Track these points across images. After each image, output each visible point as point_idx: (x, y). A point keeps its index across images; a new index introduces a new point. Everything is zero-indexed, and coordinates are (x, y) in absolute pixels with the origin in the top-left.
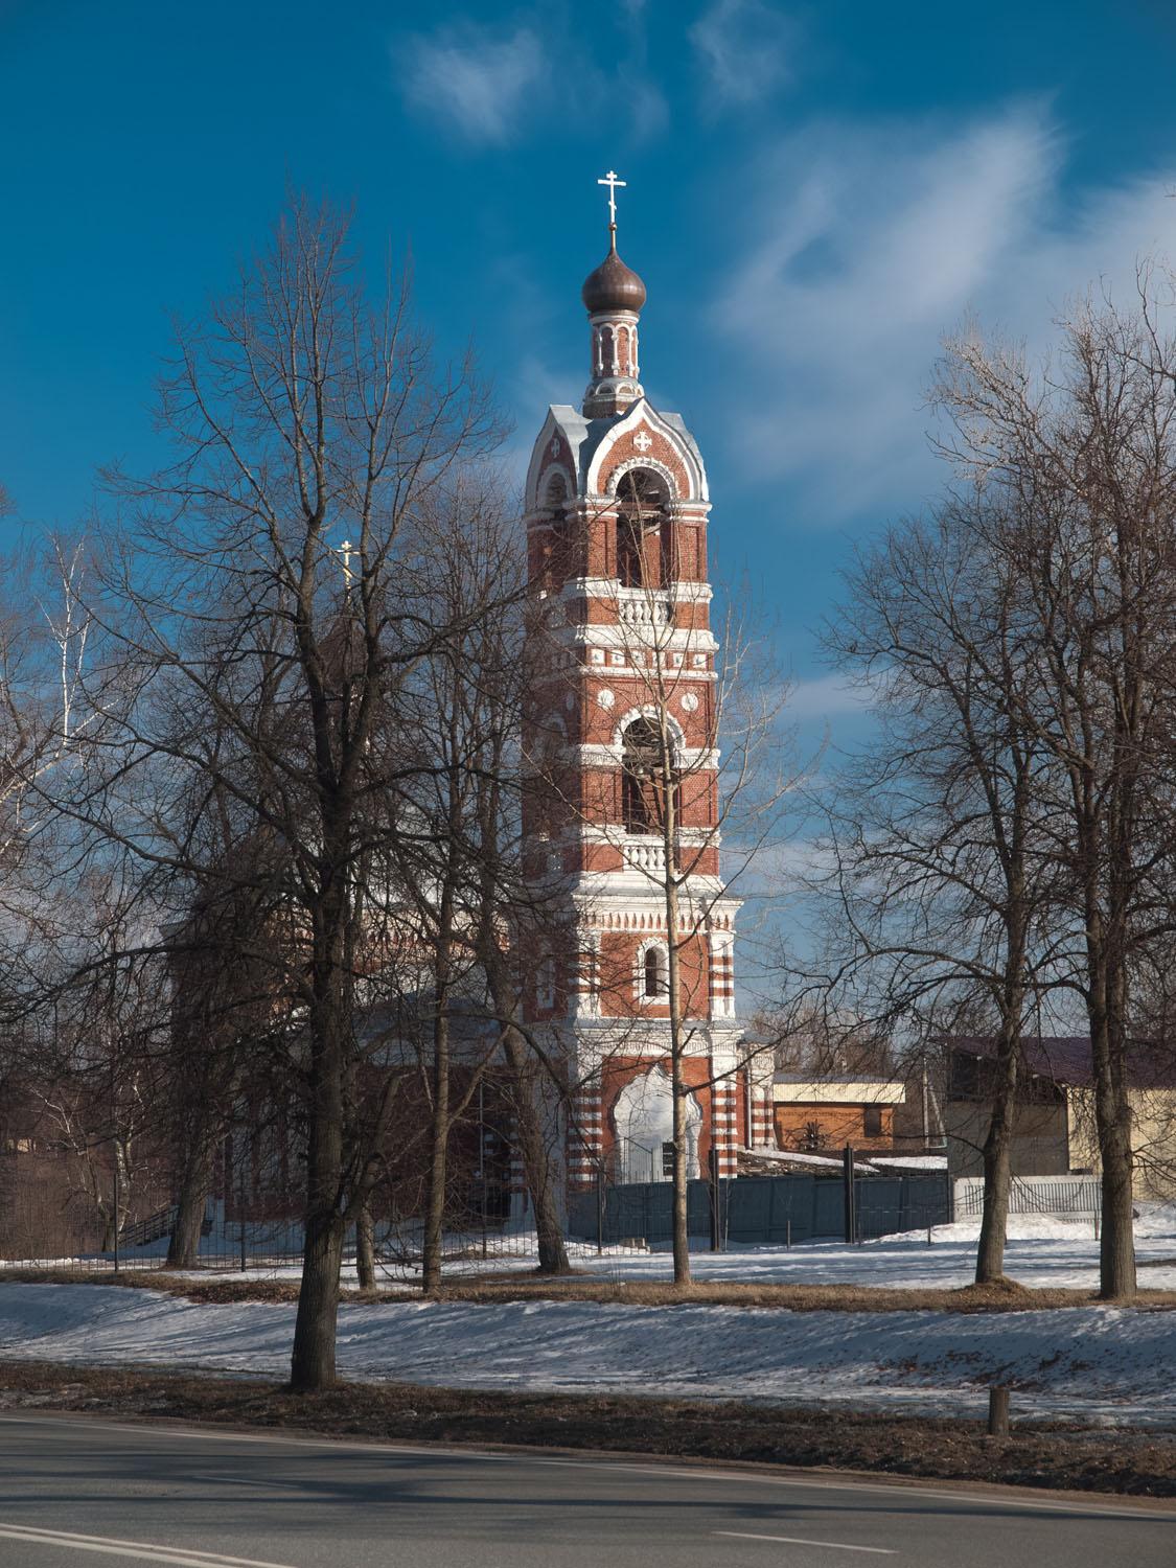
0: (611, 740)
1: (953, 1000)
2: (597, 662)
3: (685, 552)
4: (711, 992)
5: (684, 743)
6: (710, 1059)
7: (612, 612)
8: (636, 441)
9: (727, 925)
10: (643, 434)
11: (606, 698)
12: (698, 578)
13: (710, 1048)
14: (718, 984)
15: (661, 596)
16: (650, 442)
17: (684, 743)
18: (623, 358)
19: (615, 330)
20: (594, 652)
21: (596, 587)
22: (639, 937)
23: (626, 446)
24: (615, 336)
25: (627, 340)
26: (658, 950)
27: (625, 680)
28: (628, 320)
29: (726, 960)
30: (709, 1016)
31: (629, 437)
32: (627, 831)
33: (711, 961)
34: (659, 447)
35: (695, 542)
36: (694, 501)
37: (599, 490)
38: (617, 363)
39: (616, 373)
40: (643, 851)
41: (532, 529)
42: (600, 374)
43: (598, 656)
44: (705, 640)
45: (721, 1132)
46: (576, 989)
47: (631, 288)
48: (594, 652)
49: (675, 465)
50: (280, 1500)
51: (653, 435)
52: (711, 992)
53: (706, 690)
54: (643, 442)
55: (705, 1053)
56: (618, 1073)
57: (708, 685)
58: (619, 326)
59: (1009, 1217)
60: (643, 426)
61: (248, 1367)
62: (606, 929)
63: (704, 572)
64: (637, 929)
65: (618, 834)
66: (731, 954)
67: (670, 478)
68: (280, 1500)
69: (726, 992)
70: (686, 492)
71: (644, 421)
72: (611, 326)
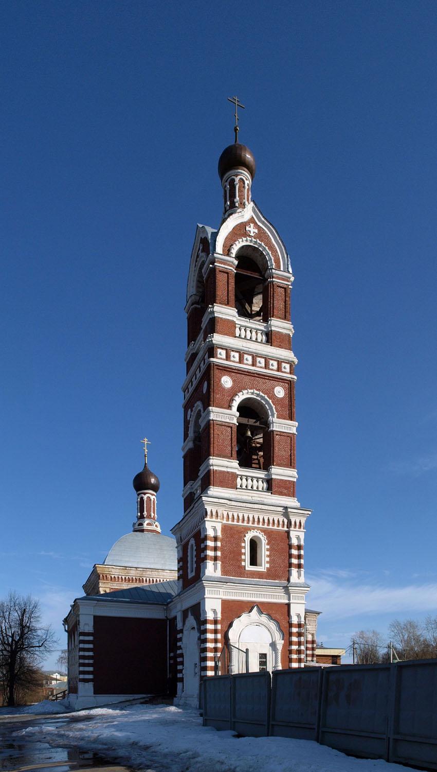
2: (220, 358)
4: (290, 565)
5: (275, 416)
6: (288, 605)
8: (248, 228)
9: (133, 581)
10: (252, 225)
11: (227, 382)
13: (289, 599)
14: (295, 561)
16: (256, 231)
17: (275, 416)
19: (237, 179)
25: (244, 187)
26: (254, 537)
28: (244, 176)
29: (215, 539)
30: (288, 580)
34: (261, 235)
35: (283, 297)
36: (282, 273)
37: (223, 251)
39: (237, 205)
40: (255, 480)
41: (212, 365)
42: (228, 208)
43: (222, 353)
45: (294, 647)
46: (205, 558)
48: (219, 351)
52: (290, 565)
53: (290, 385)
54: (252, 230)
55: (287, 601)
56: (233, 610)
57: (290, 382)
58: (239, 177)
60: (252, 220)
61: (85, 714)
62: (225, 522)
64: (245, 524)
65: (231, 465)
66: (302, 543)
67: (267, 252)
69: (299, 566)
71: (253, 217)
72: (235, 177)
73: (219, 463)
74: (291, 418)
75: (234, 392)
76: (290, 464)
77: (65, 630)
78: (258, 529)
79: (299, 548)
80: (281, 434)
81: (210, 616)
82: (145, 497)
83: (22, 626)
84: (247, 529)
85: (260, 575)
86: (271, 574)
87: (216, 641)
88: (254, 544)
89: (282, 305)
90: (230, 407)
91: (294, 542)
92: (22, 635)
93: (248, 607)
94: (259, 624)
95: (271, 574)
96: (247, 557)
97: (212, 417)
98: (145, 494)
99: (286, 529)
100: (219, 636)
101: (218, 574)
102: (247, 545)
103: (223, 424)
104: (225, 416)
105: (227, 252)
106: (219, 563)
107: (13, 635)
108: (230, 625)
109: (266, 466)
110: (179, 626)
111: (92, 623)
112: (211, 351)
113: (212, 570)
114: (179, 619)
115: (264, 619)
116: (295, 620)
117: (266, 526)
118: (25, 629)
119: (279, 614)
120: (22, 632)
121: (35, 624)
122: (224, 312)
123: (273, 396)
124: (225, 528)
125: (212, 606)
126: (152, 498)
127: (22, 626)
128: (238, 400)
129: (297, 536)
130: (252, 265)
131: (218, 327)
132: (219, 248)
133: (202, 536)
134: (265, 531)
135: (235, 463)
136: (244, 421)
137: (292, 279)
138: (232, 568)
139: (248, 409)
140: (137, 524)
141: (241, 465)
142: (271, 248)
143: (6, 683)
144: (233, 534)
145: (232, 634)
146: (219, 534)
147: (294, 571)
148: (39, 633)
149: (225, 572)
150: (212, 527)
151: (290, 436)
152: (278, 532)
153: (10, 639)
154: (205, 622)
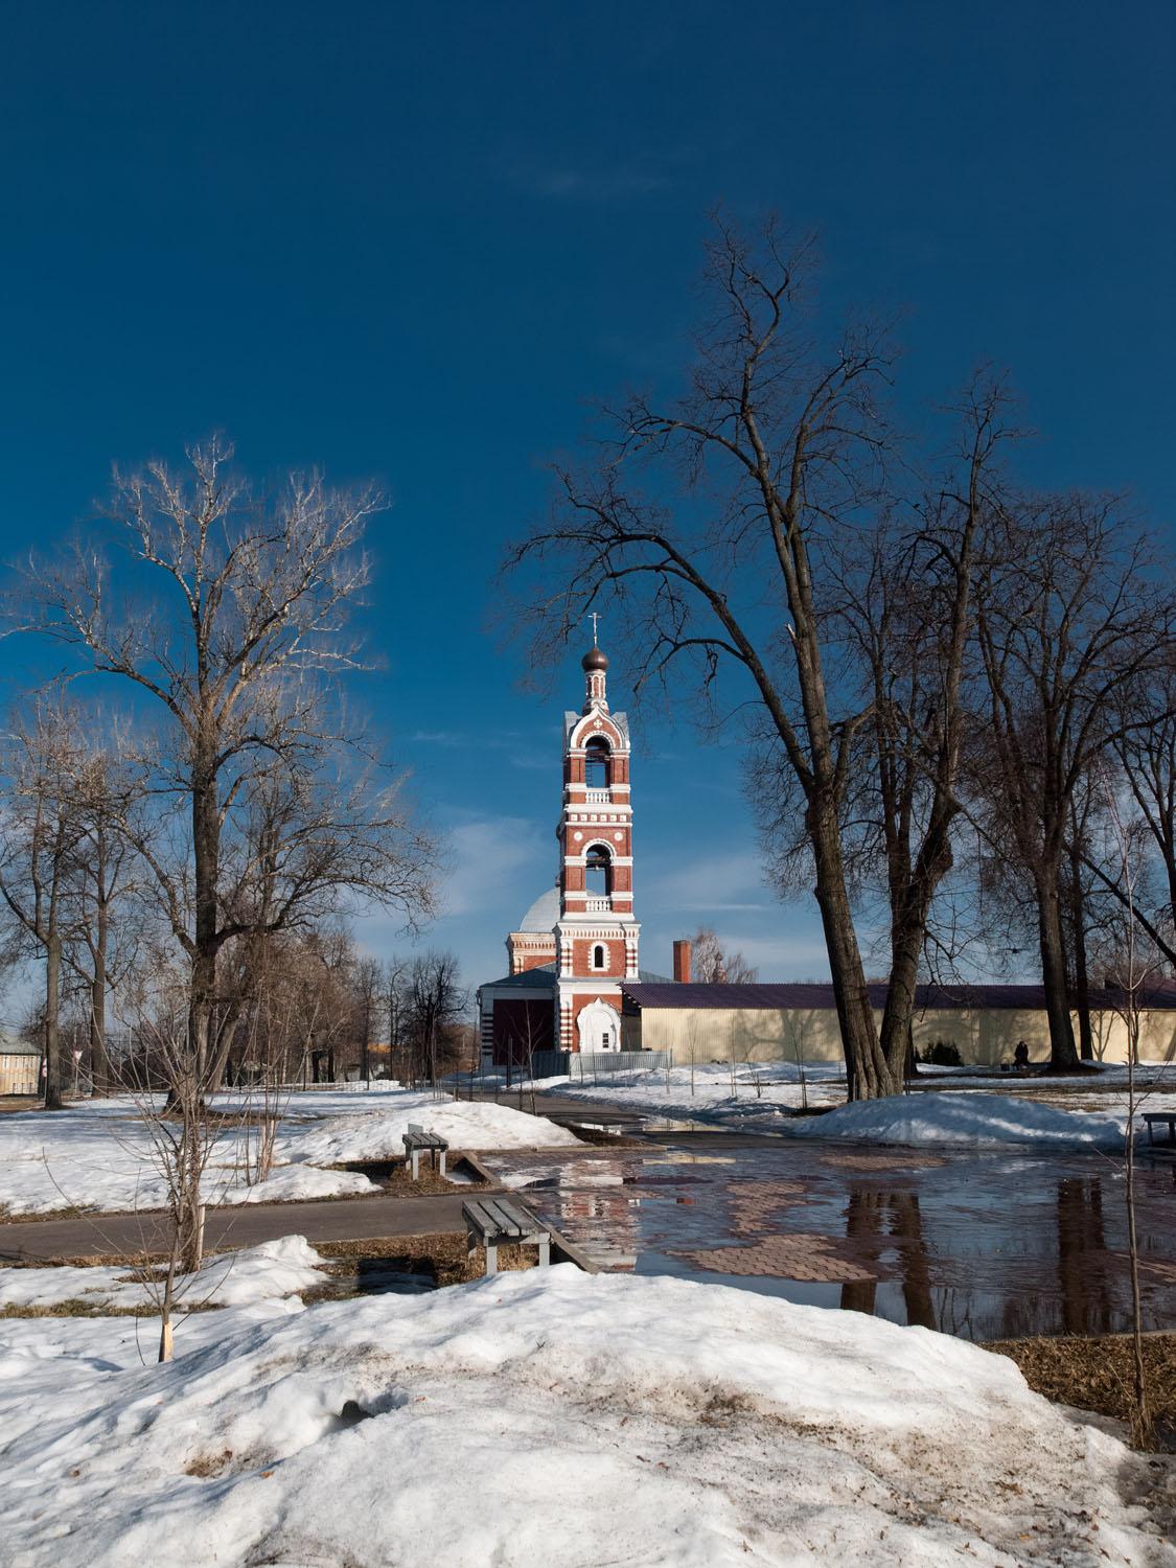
0: (580, 854)
1: (214, 780)
3: (617, 772)
7: (582, 798)
11: (578, 836)
12: (623, 782)
14: (629, 962)
15: (606, 790)
19: (593, 678)
21: (573, 787)
22: (592, 941)
23: (590, 726)
24: (593, 680)
27: (587, 828)
28: (600, 674)
29: (634, 951)
31: (591, 722)
32: (588, 786)
33: (626, 951)
34: (605, 726)
36: (622, 748)
38: (593, 692)
44: (628, 809)
47: (601, 660)
49: (612, 732)
50: (579, 921)
51: (603, 721)
54: (598, 724)
56: (581, 1001)
57: (627, 828)
59: (888, 1135)
60: (598, 717)
63: (627, 779)
68: (579, 921)
69: (634, 965)
70: (618, 744)
74: (628, 855)
75: (583, 843)
76: (627, 889)
77: (260, 1405)
80: (620, 867)
81: (564, 1006)
83: (441, 987)
84: (592, 941)
86: (612, 973)
87: (568, 1025)
88: (599, 951)
89: (621, 772)
91: (629, 947)
92: (440, 997)
94: (603, 1011)
95: (612, 973)
100: (571, 1021)
101: (570, 975)
106: (571, 968)
107: (430, 996)
111: (492, 1005)
112: (567, 817)
115: (606, 1007)
118: (443, 990)
120: (440, 993)
121: (453, 983)
123: (612, 841)
124: (576, 942)
125: (566, 1000)
127: (441, 987)
128: (586, 848)
129: (632, 943)
130: (599, 745)
131: (572, 799)
134: (606, 941)
138: (581, 971)
143: (410, 1050)
144: (581, 946)
146: (571, 947)
147: (629, 969)
148: (458, 994)
149: (575, 974)
151: (627, 868)
152: (617, 942)
153: (427, 1002)
154: (561, 1011)
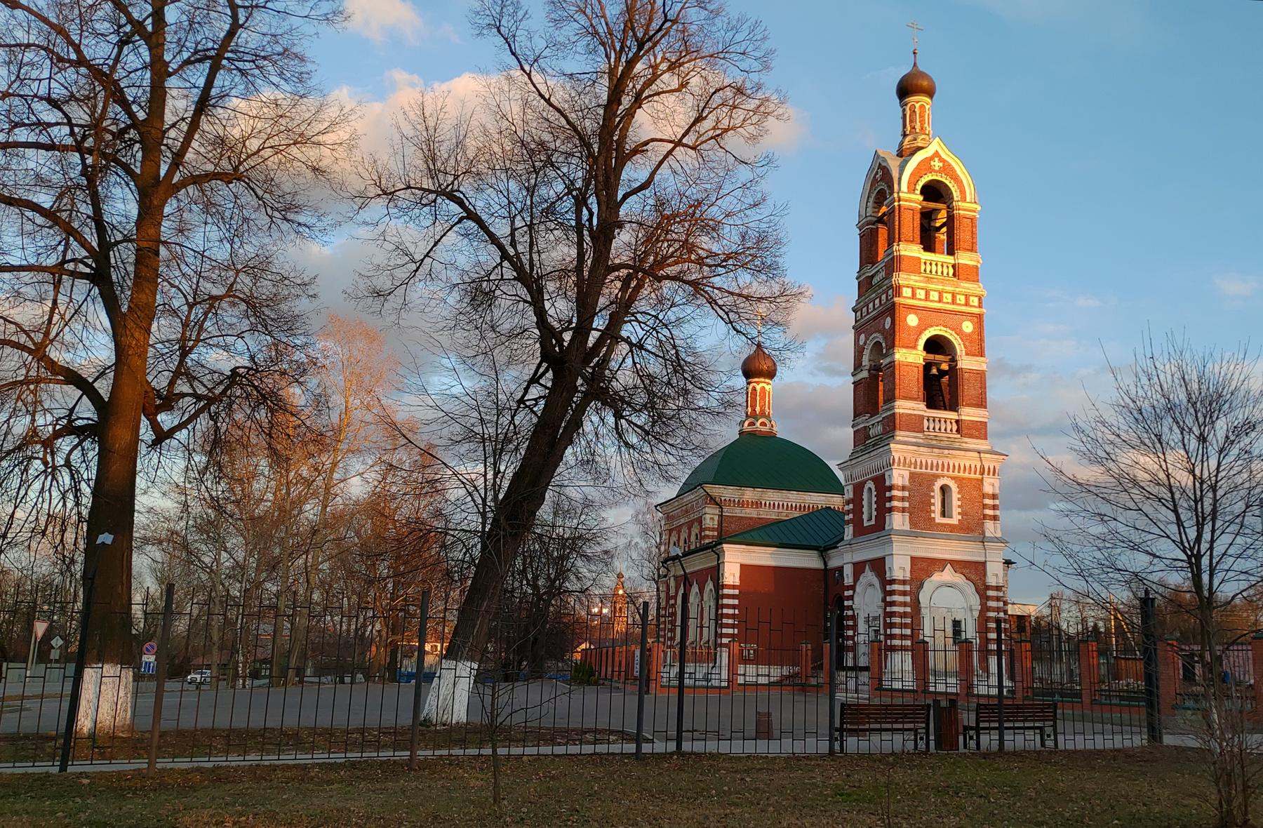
6: (984, 564)
11: (912, 320)
18: (922, 122)
20: (904, 289)
27: (925, 309)
36: (967, 202)
43: (907, 292)
54: (937, 164)
55: (982, 559)
56: (923, 568)
60: (936, 154)
73: (908, 407)
78: (953, 478)
79: (994, 497)
80: (971, 371)
82: (758, 387)
84: (937, 477)
85: (952, 528)
88: (944, 489)
90: (915, 347)
93: (940, 564)
96: (937, 507)
97: (897, 356)
98: (758, 383)
99: (978, 476)
102: (956, 511)
103: (909, 365)
104: (910, 357)
105: (911, 190)
108: (921, 586)
109: (953, 407)
110: (848, 581)
113: (898, 521)
114: (848, 571)
116: (991, 581)
117: (956, 473)
119: (974, 571)
122: (910, 250)
123: (960, 332)
124: (913, 476)
126: (767, 387)
132: (904, 187)
133: (887, 484)
134: (958, 480)
135: (922, 406)
136: (931, 357)
137: (979, 208)
139: (936, 345)
140: (746, 424)
141: (929, 406)
142: (956, 179)
144: (921, 483)
145: (923, 597)
149: (913, 523)
150: (899, 477)
